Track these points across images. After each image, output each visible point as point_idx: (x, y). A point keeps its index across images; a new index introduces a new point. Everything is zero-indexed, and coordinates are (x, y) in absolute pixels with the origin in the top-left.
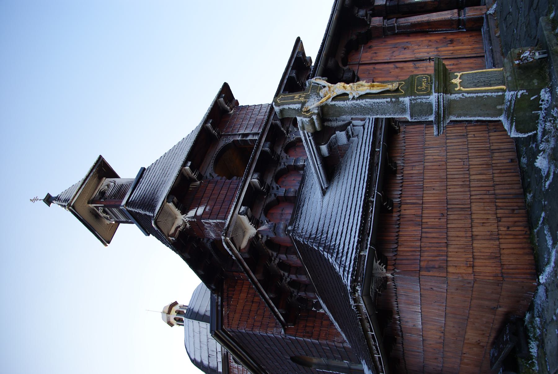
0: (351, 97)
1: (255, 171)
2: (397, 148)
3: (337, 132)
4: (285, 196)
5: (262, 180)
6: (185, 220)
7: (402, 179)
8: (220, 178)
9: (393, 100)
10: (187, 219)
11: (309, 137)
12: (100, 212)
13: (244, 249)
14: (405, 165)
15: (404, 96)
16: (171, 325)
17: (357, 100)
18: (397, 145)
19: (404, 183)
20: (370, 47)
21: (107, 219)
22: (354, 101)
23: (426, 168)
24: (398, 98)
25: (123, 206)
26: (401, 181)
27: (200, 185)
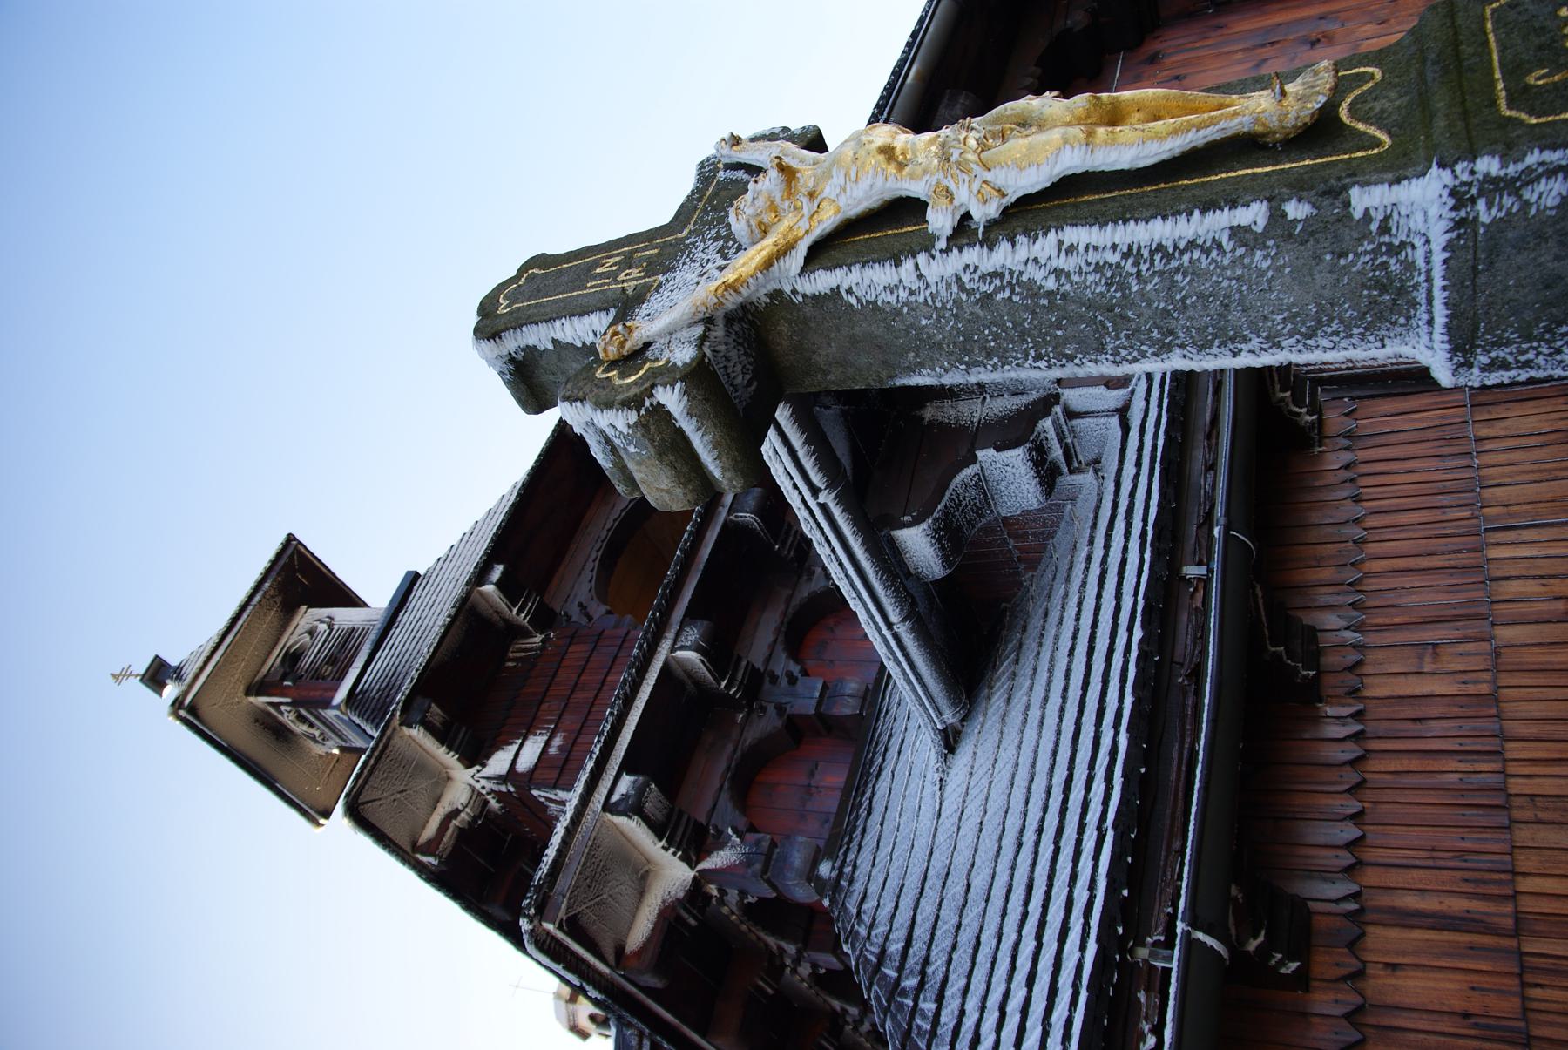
0: (940, 221)
1: (691, 615)
2: (1313, 535)
3: (986, 455)
4: (819, 714)
5: (718, 651)
6: (478, 786)
7: (1357, 737)
8: (613, 619)
9: (1296, 210)
10: (483, 782)
11: (815, 491)
12: (287, 717)
13: (638, 954)
14: (1372, 639)
15: (1398, 167)
16: (584, 1035)
17: (989, 243)
18: (1315, 517)
19: (1374, 765)
20: (1153, 59)
21: (314, 738)
22: (972, 255)
23: (1508, 657)
24: (1337, 193)
25: (338, 707)
26: (1350, 751)
27: (542, 648)
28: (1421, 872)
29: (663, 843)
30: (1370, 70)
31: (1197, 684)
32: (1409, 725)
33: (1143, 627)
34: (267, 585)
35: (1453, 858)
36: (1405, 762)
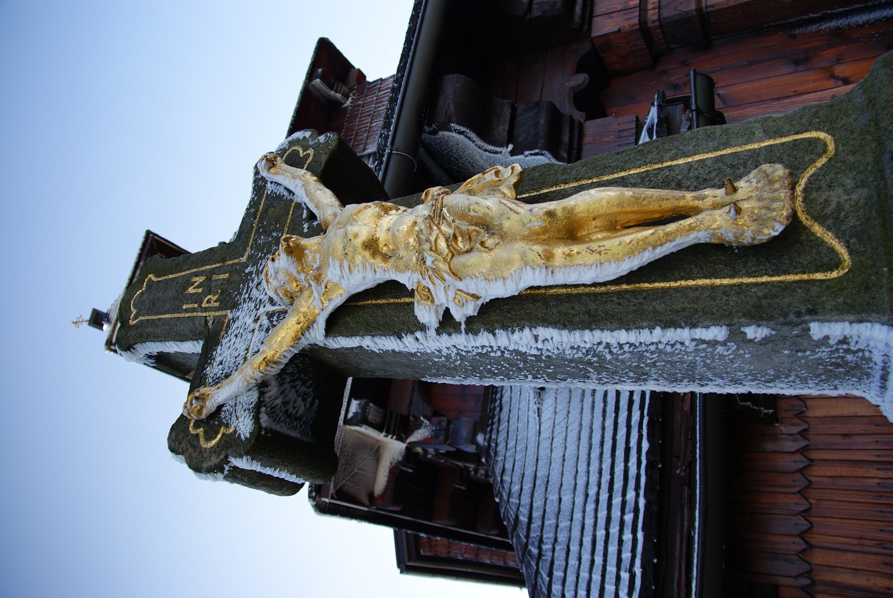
7: (803, 451)
13: (383, 495)
26: (799, 461)
28: (853, 555)
29: (384, 433)
30: (822, 135)
31: (690, 488)
32: (840, 439)
33: (649, 439)
34: (141, 263)
35: (876, 545)
36: (839, 469)
